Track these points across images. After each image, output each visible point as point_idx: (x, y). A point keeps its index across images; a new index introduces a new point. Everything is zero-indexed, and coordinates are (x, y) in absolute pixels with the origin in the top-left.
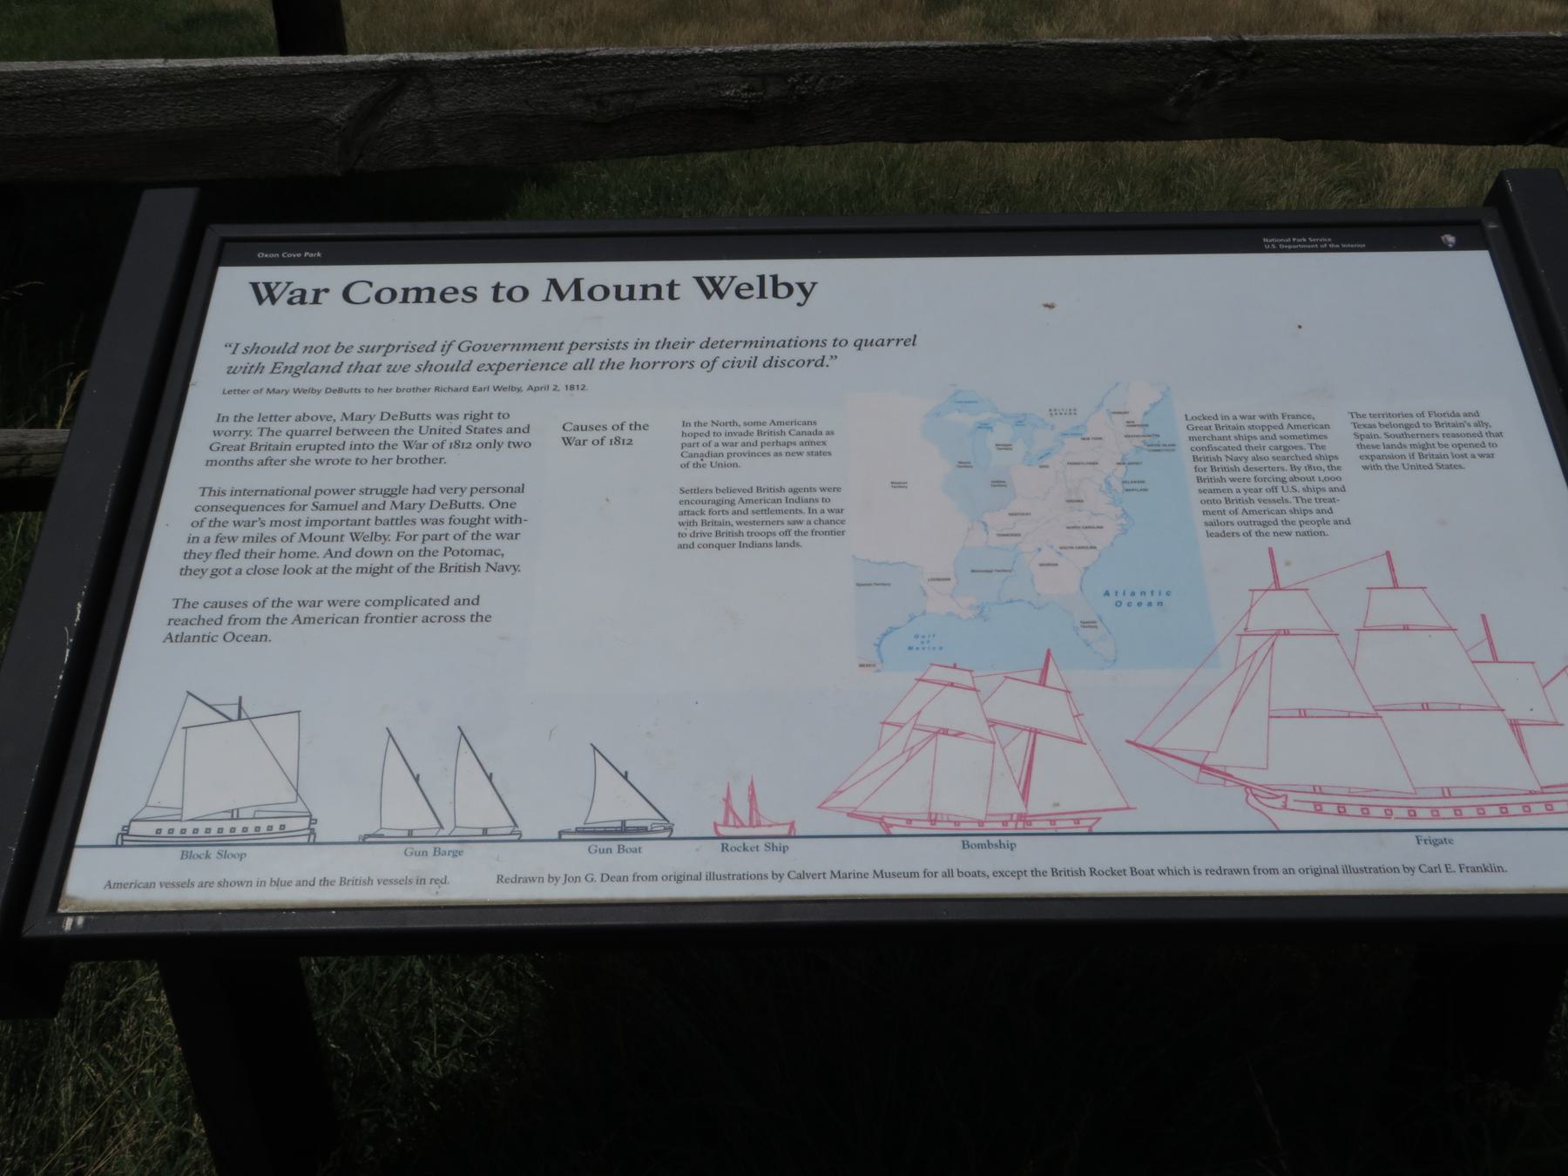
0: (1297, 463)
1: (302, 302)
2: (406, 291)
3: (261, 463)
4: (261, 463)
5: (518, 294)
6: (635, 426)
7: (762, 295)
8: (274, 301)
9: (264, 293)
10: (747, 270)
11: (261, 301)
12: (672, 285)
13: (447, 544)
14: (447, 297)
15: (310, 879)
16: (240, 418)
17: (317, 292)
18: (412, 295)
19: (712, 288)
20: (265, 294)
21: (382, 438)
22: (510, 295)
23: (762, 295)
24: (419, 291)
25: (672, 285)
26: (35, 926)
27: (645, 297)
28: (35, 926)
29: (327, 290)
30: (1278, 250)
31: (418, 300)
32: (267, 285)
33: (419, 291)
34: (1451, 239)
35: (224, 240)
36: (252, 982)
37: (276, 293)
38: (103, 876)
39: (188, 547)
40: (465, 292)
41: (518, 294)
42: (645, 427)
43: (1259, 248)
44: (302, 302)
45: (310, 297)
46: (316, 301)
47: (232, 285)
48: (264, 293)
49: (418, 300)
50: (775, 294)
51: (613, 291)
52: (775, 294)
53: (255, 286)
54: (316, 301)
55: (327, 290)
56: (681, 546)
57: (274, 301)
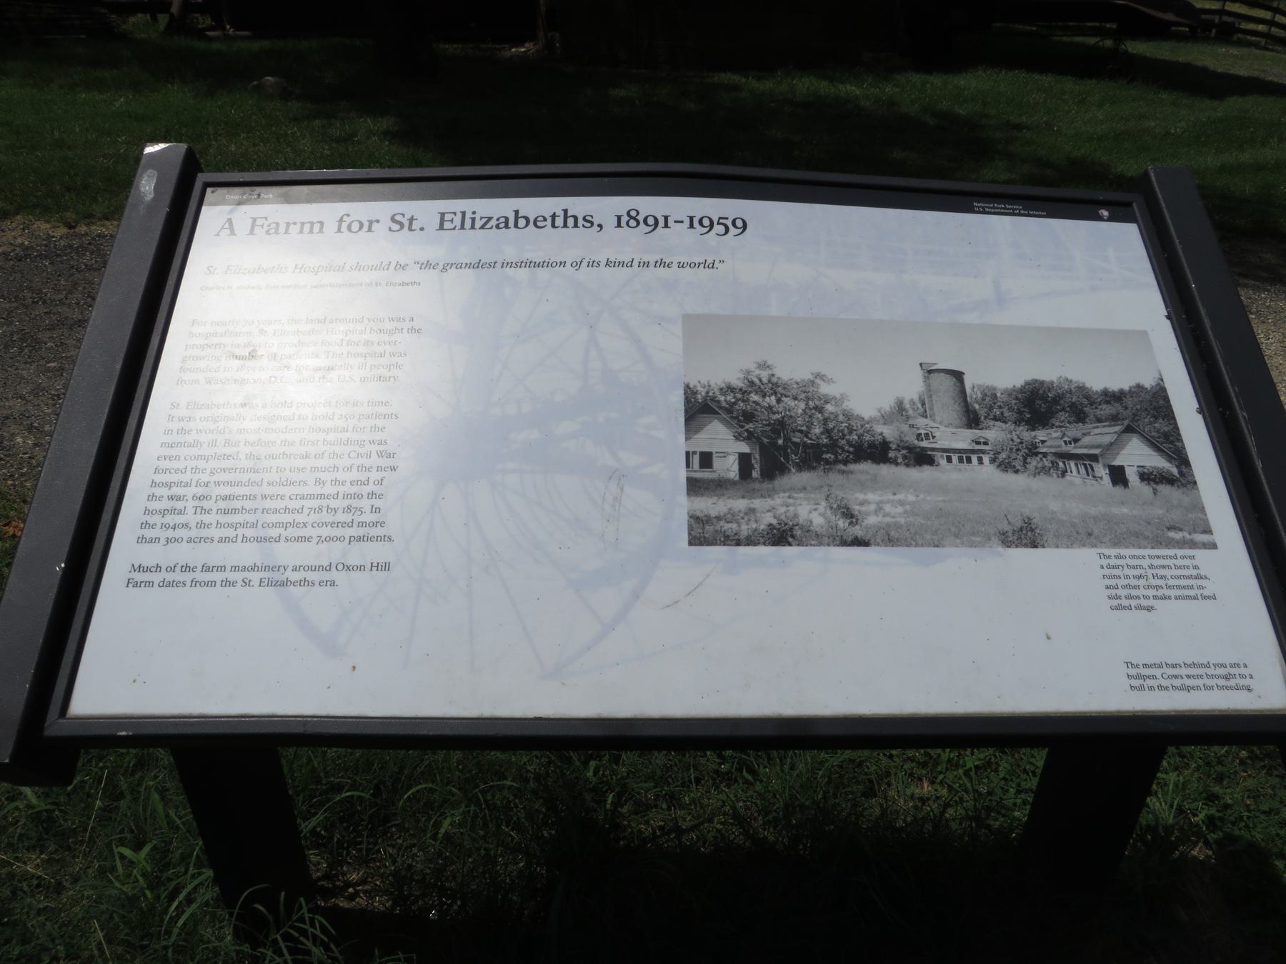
0: (323, 476)
1: (507, 227)
7: (462, 227)
14: (539, 224)
15: (325, 564)
17: (371, 223)
18: (307, 227)
22: (349, 228)
23: (462, 227)
24: (312, 224)
26: (54, 726)
28: (54, 726)
29: (378, 221)
30: (984, 212)
31: (311, 232)
33: (312, 224)
34: (1105, 213)
36: (240, 779)
39: (141, 533)
40: (592, 224)
44: (507, 227)
45: (282, 228)
46: (286, 232)
49: (311, 232)
50: (516, 226)
52: (516, 226)
54: (370, 230)
55: (378, 221)
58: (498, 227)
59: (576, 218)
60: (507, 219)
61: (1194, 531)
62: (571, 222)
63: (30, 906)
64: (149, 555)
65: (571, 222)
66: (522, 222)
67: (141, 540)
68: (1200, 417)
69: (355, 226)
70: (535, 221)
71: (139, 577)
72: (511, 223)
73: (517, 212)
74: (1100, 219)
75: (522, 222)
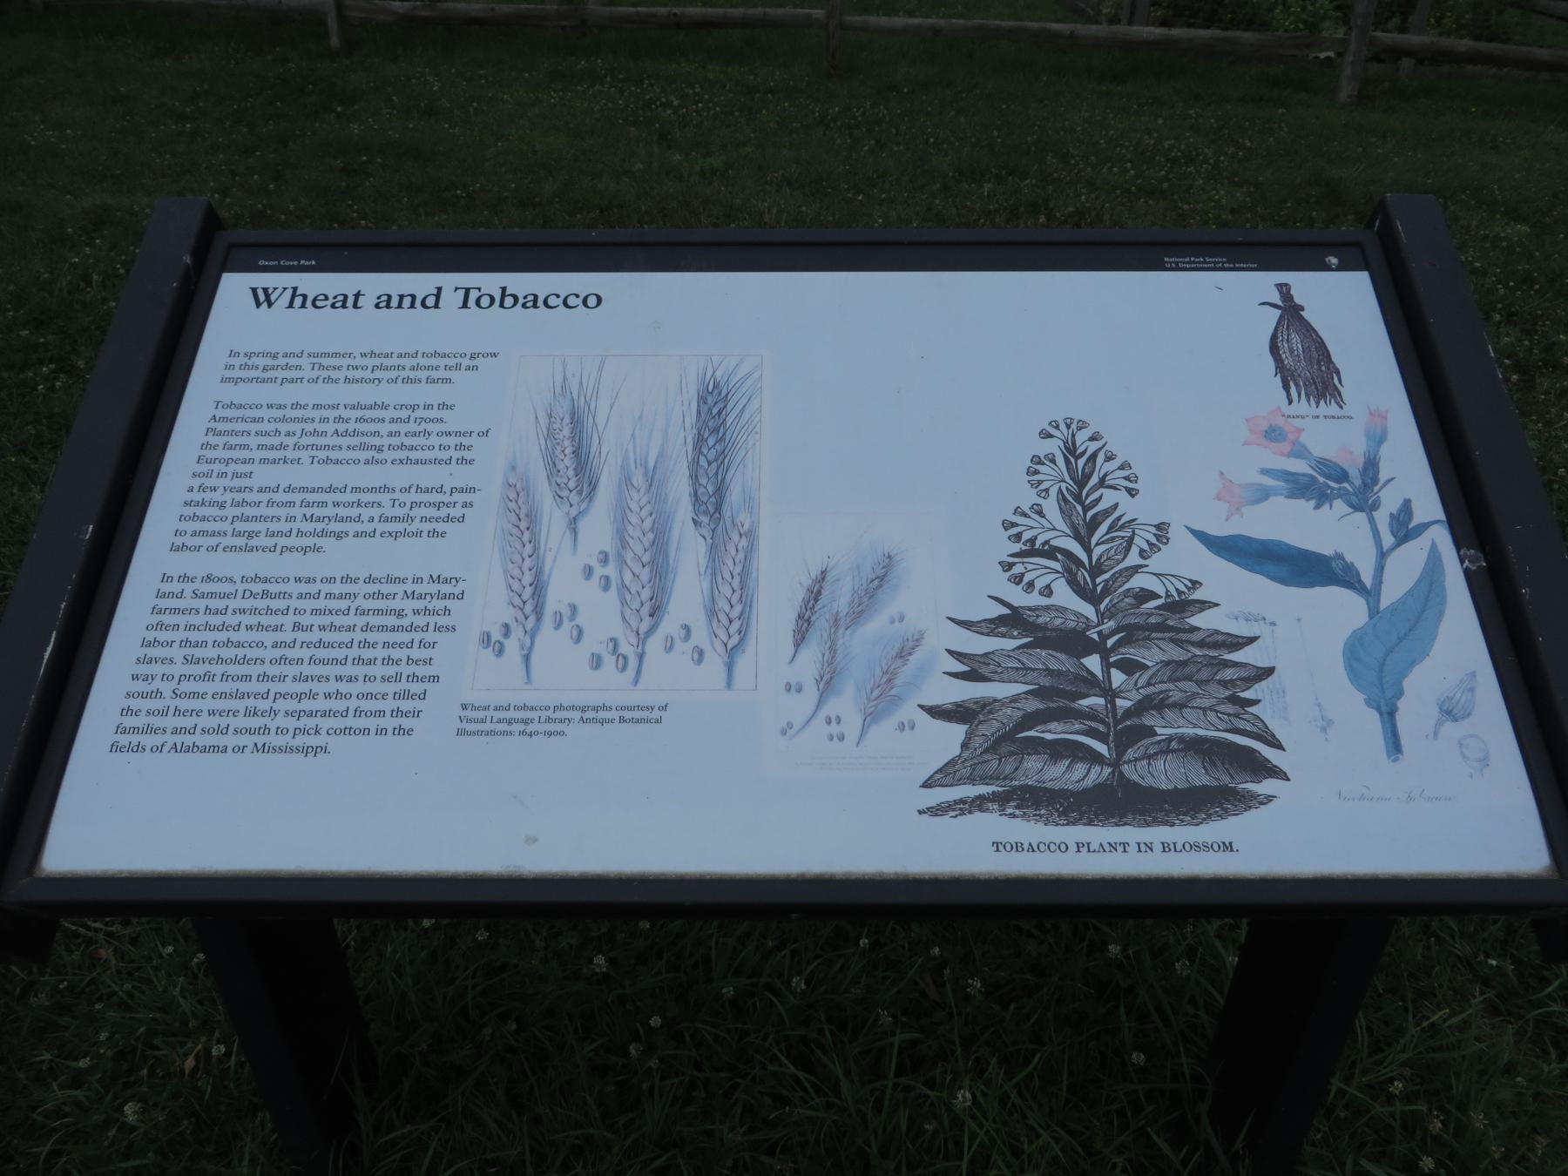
1: (388, 306)
2: (401, 297)
3: (367, 462)
4: (367, 462)
5: (592, 301)
6: (443, 406)
8: (270, 305)
9: (262, 297)
10: (490, 282)
11: (258, 304)
12: (357, 295)
13: (394, 496)
14: (319, 303)
16: (297, 406)
19: (297, 298)
20: (264, 298)
21: (336, 413)
22: (492, 299)
25: (357, 295)
27: (400, 306)
30: (1178, 269)
32: (265, 290)
34: (1334, 261)
35: (232, 246)
37: (273, 298)
38: (120, 815)
41: (592, 301)
42: (451, 407)
43: (1160, 267)
44: (388, 306)
46: (355, 306)
47: (234, 288)
48: (262, 297)
50: (502, 305)
51: (418, 303)
52: (502, 305)
53: (254, 290)
56: (473, 490)
57: (270, 305)
58: (333, 306)
59: (305, 297)
60: (346, 297)
61: (996, 760)
62: (298, 301)
63: (1102, 616)
64: (180, 564)
65: (298, 301)
66: (509, 301)
67: (175, 548)
68: (1327, 551)
69: (485, 301)
70: (315, 300)
71: (124, 740)
72: (350, 302)
73: (504, 289)
74: (1328, 268)
75: (509, 301)
